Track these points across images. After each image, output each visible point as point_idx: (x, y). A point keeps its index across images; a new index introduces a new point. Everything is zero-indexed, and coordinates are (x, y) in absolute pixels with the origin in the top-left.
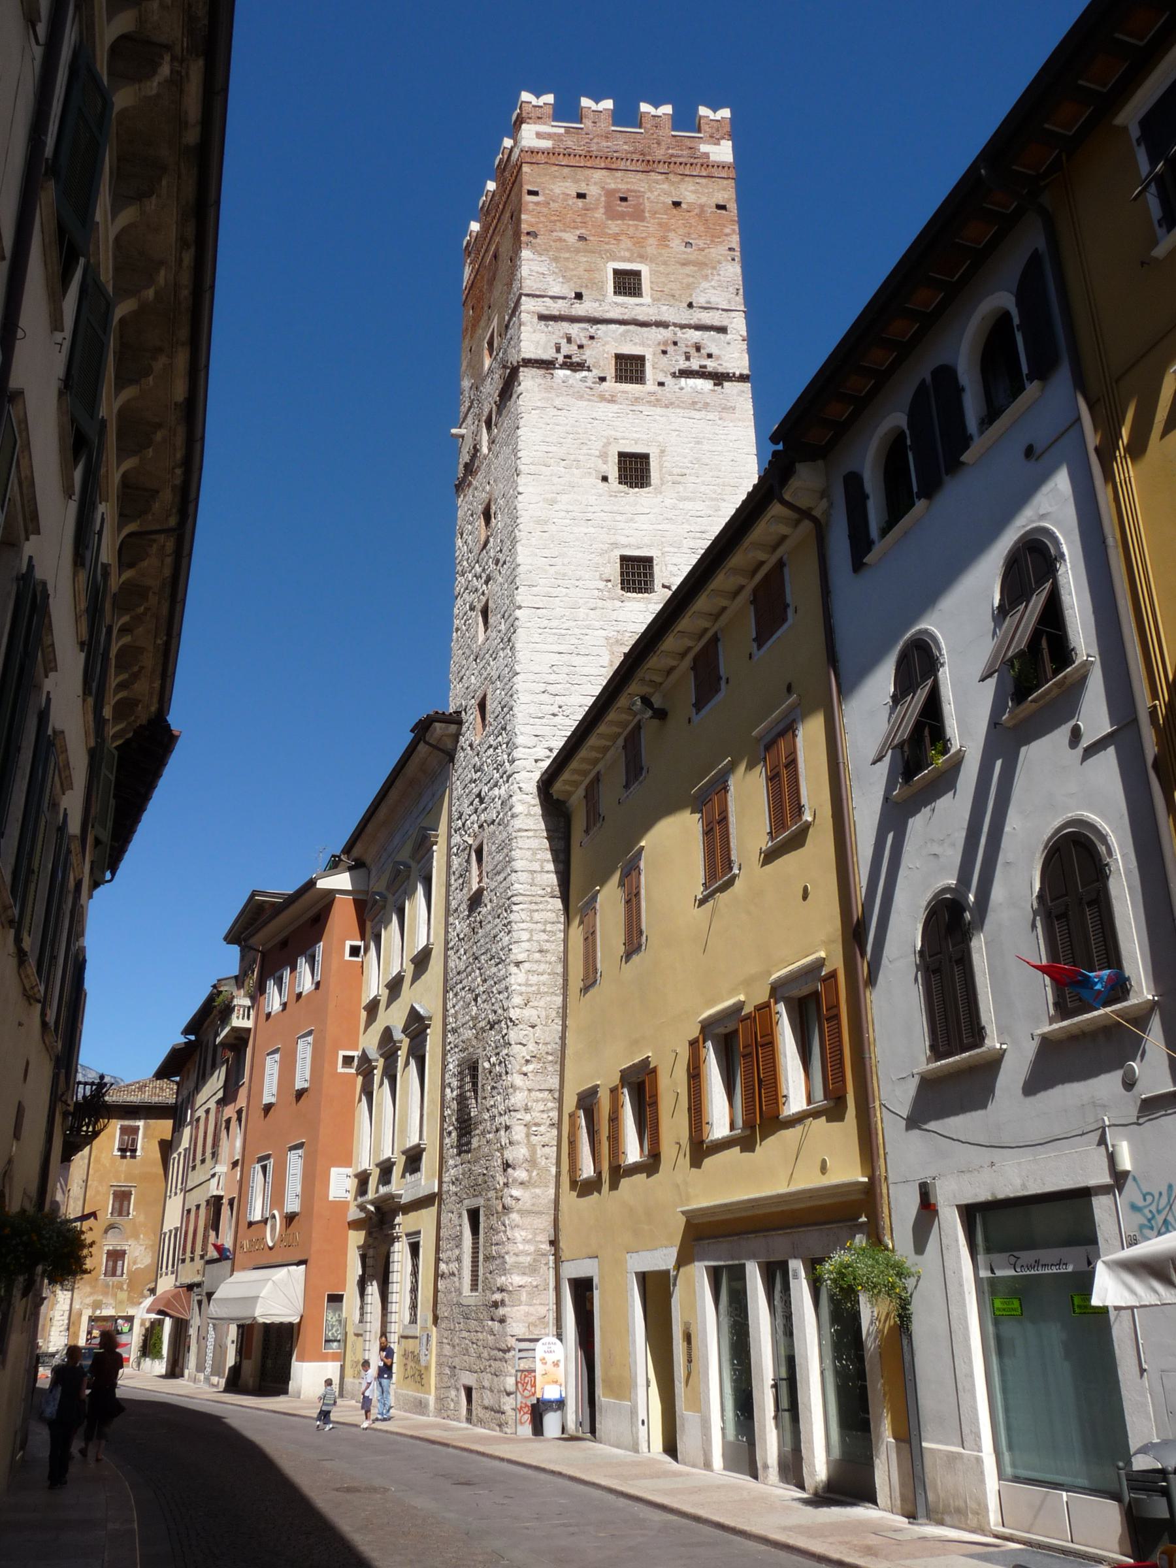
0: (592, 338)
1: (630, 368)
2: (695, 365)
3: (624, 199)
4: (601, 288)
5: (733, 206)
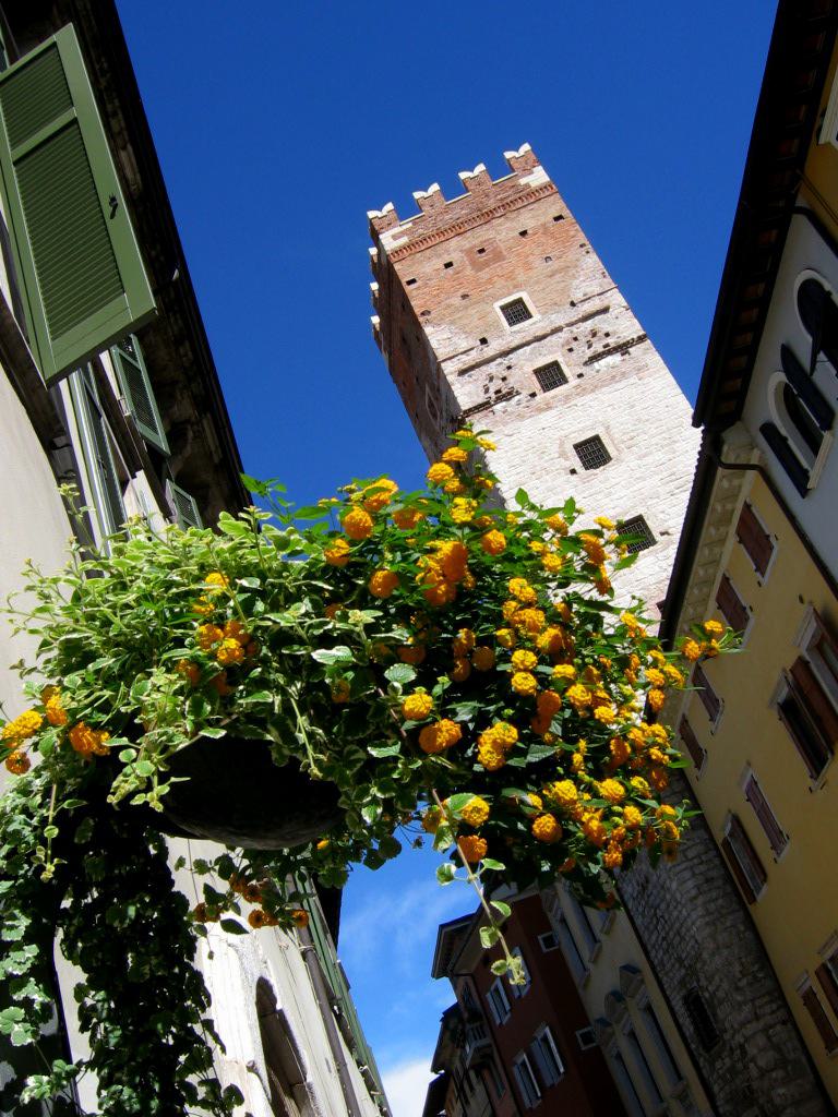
0: (509, 368)
1: (550, 376)
2: (598, 347)
3: (482, 251)
4: (498, 326)
5: (566, 213)
